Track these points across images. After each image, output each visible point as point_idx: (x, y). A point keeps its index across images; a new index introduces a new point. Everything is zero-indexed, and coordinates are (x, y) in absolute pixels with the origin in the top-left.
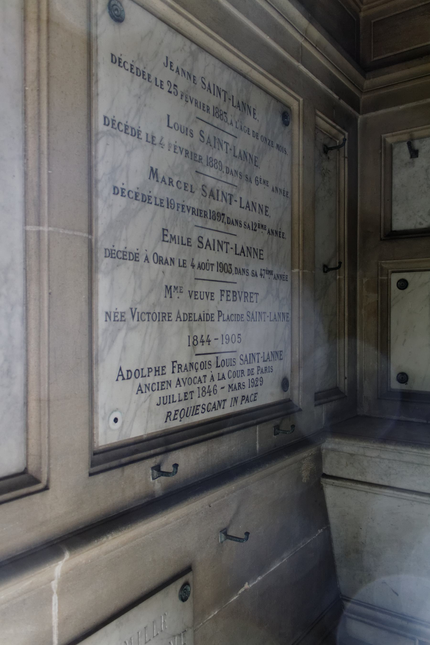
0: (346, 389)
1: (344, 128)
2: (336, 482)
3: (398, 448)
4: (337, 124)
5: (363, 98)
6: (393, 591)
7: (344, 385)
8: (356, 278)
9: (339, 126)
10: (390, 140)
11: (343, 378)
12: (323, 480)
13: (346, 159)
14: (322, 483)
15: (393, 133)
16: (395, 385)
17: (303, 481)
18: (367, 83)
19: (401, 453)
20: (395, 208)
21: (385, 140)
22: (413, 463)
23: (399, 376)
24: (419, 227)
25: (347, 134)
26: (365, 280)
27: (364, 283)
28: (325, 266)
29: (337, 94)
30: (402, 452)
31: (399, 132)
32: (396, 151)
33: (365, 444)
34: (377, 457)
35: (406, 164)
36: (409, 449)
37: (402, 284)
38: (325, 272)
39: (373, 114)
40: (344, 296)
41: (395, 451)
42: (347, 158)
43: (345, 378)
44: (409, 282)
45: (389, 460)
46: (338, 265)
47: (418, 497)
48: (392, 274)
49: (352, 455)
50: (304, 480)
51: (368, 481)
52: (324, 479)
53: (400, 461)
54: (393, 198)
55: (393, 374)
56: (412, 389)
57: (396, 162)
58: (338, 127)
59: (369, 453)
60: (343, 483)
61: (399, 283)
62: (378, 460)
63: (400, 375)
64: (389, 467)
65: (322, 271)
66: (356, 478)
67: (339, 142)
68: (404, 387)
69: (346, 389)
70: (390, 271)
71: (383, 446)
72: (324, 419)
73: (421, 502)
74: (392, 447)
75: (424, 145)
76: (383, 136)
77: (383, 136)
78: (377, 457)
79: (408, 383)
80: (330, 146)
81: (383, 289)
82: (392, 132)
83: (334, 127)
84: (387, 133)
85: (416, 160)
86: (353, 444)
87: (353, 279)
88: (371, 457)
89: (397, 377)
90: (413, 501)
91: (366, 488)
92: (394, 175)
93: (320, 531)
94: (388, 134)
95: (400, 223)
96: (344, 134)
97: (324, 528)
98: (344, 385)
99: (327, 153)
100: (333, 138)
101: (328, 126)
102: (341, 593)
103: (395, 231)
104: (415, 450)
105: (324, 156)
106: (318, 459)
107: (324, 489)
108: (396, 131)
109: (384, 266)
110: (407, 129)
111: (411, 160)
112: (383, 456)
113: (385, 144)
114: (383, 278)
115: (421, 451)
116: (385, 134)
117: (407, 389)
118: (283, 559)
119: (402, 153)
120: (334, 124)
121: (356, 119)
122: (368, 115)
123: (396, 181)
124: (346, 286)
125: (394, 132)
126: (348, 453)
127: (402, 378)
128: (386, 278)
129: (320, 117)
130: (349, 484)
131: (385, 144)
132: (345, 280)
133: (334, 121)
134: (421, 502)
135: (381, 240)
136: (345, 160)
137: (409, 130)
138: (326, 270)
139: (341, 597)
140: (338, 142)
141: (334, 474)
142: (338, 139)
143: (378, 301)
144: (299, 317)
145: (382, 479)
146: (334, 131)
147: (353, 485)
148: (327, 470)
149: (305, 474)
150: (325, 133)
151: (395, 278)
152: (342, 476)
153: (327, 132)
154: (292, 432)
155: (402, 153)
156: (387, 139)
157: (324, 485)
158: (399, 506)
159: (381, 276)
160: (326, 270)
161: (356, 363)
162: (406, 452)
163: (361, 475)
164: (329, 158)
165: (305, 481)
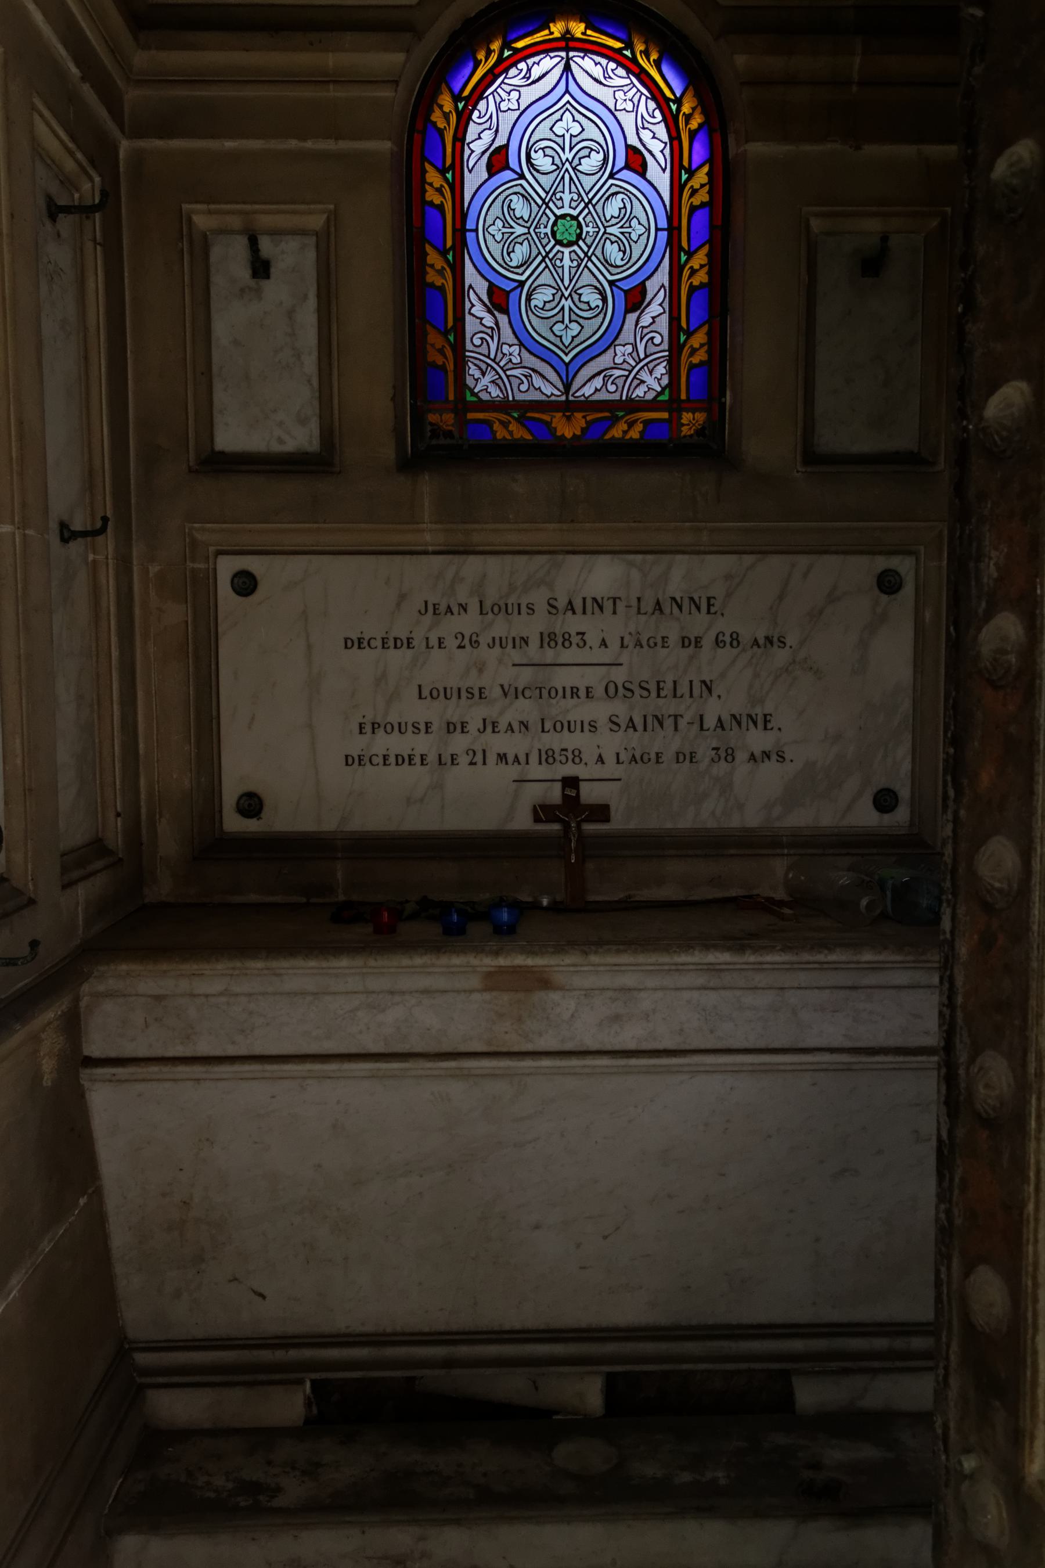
0: (120, 843)
1: (92, 162)
2: (120, 1071)
3: (274, 964)
4: (79, 147)
5: (131, 95)
6: (255, 1292)
7: (115, 833)
8: (131, 563)
9: (84, 154)
10: (202, 221)
11: (111, 815)
12: (85, 1074)
13: (98, 247)
14: (82, 1082)
15: (212, 207)
16: (233, 823)
17: (45, 1084)
18: (140, 59)
19: (280, 975)
20: (220, 396)
21: (190, 220)
22: (303, 994)
23: (242, 801)
24: (276, 448)
25: (97, 179)
26: (154, 569)
27: (151, 575)
28: (63, 526)
29: (78, 65)
30: (283, 971)
31: (228, 207)
32: (216, 252)
33: (195, 967)
34: (221, 994)
35: (242, 290)
36: (299, 962)
37: (244, 583)
38: (64, 540)
39: (159, 143)
40: (108, 608)
41: (266, 972)
42: (99, 244)
43: (118, 815)
44: (258, 578)
45: (250, 995)
46: (99, 524)
47: (317, 1067)
48: (220, 557)
49: (158, 998)
50: (47, 1081)
51: (199, 1054)
52: (88, 1071)
53: (274, 994)
54: (215, 369)
55: (230, 796)
56: (273, 830)
57: (219, 282)
58: (79, 155)
59: (203, 987)
60: (139, 1070)
61: (236, 580)
62: (223, 999)
63: (244, 798)
64: (251, 1013)
65: (58, 539)
66: (170, 1053)
67: (80, 198)
68: (252, 826)
69: (120, 843)
70: (212, 549)
71: (238, 964)
72: (81, 919)
73: (323, 1077)
74: (259, 964)
75: (283, 252)
76: (185, 207)
77: (185, 207)
78: (221, 994)
79: (263, 815)
80: (62, 202)
81: (199, 592)
82: (209, 203)
83: (71, 153)
84: (196, 202)
85: (265, 284)
86: (165, 972)
87: (124, 564)
88: (207, 996)
89: (238, 803)
90: (304, 1078)
91: (198, 1070)
92: (215, 316)
93: (82, 1201)
94: (199, 206)
95: (232, 436)
96: (91, 179)
97: (90, 1191)
98: (115, 833)
99: (55, 221)
100: (67, 182)
101: (56, 143)
102: (126, 1338)
103: (222, 453)
104: (312, 963)
105: (49, 225)
106: (73, 1025)
107: (87, 1096)
108: (219, 203)
109: (198, 536)
110: (244, 203)
111: (252, 283)
112: (236, 989)
113: (190, 228)
114: (197, 566)
115: (324, 964)
116: (190, 203)
117: (260, 830)
118: (9, 1294)
119: (230, 260)
120: (71, 145)
121: (116, 148)
122: (142, 144)
123: (221, 329)
124: (112, 582)
125: (214, 203)
126: (150, 996)
127: (250, 805)
128: (202, 566)
129: (41, 116)
130: (154, 1069)
131: (190, 228)
132: (107, 565)
133: (73, 139)
134: (323, 1077)
135: (190, 470)
136: (96, 249)
137: (248, 207)
138: (66, 535)
139: (127, 1346)
140: (77, 196)
141: (113, 1054)
142: (77, 190)
143: (187, 622)
144: (19, 658)
145: (233, 1043)
146: (70, 165)
147: (166, 1070)
148: (94, 1048)
149: (48, 1066)
150: (49, 162)
151: (227, 567)
152: (134, 1055)
153: (53, 161)
154: (33, 959)
155: (230, 260)
156: (196, 218)
157: (86, 1084)
158: (273, 1097)
159: (193, 561)
160: (66, 535)
161: (137, 776)
162: (290, 971)
163: (182, 1043)
164: (59, 235)
165: (50, 1084)
